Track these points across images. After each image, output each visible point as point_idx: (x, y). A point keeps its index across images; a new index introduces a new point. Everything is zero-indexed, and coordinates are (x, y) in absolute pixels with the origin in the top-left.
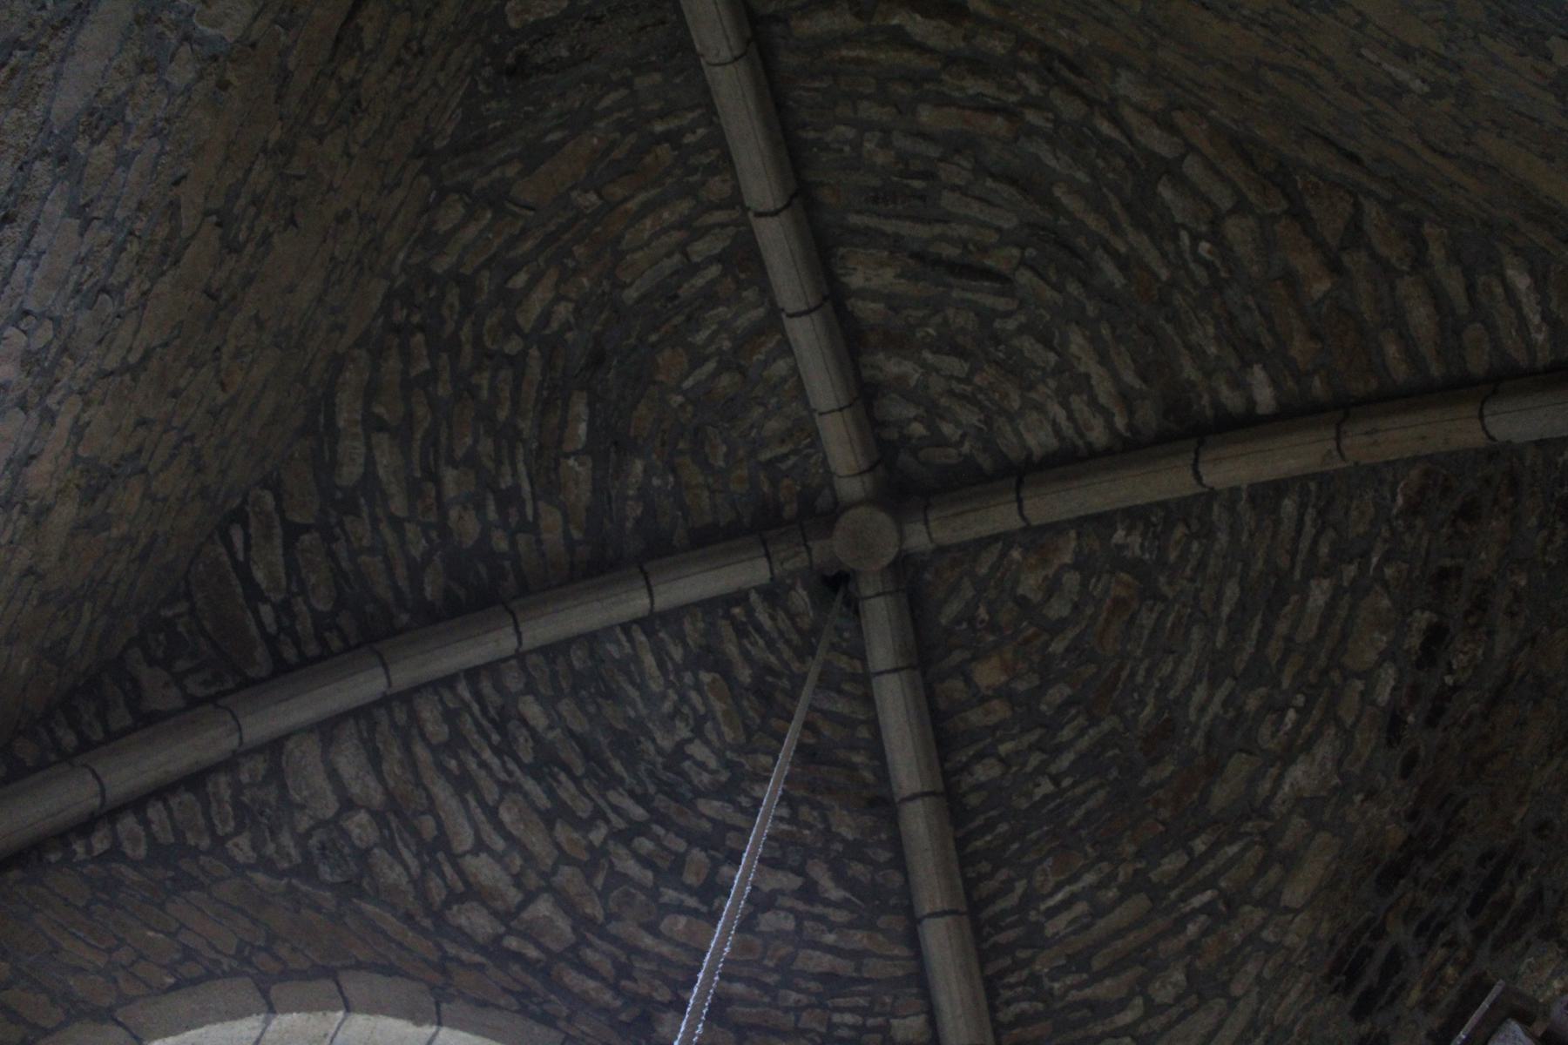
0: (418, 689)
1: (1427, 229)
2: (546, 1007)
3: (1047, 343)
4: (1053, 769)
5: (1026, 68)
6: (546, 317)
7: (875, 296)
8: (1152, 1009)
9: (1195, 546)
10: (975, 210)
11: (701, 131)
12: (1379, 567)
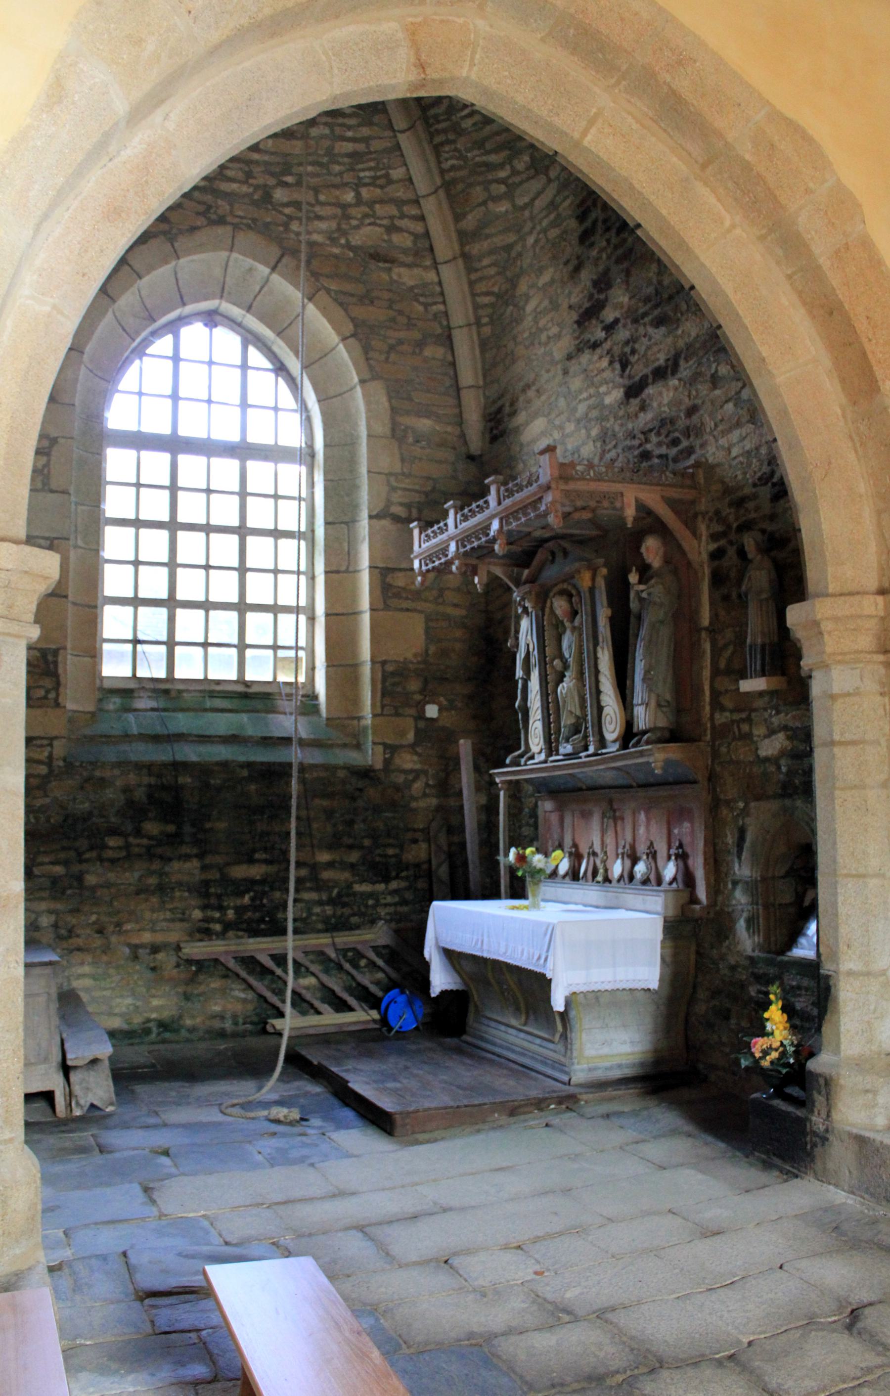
8: (515, 172)
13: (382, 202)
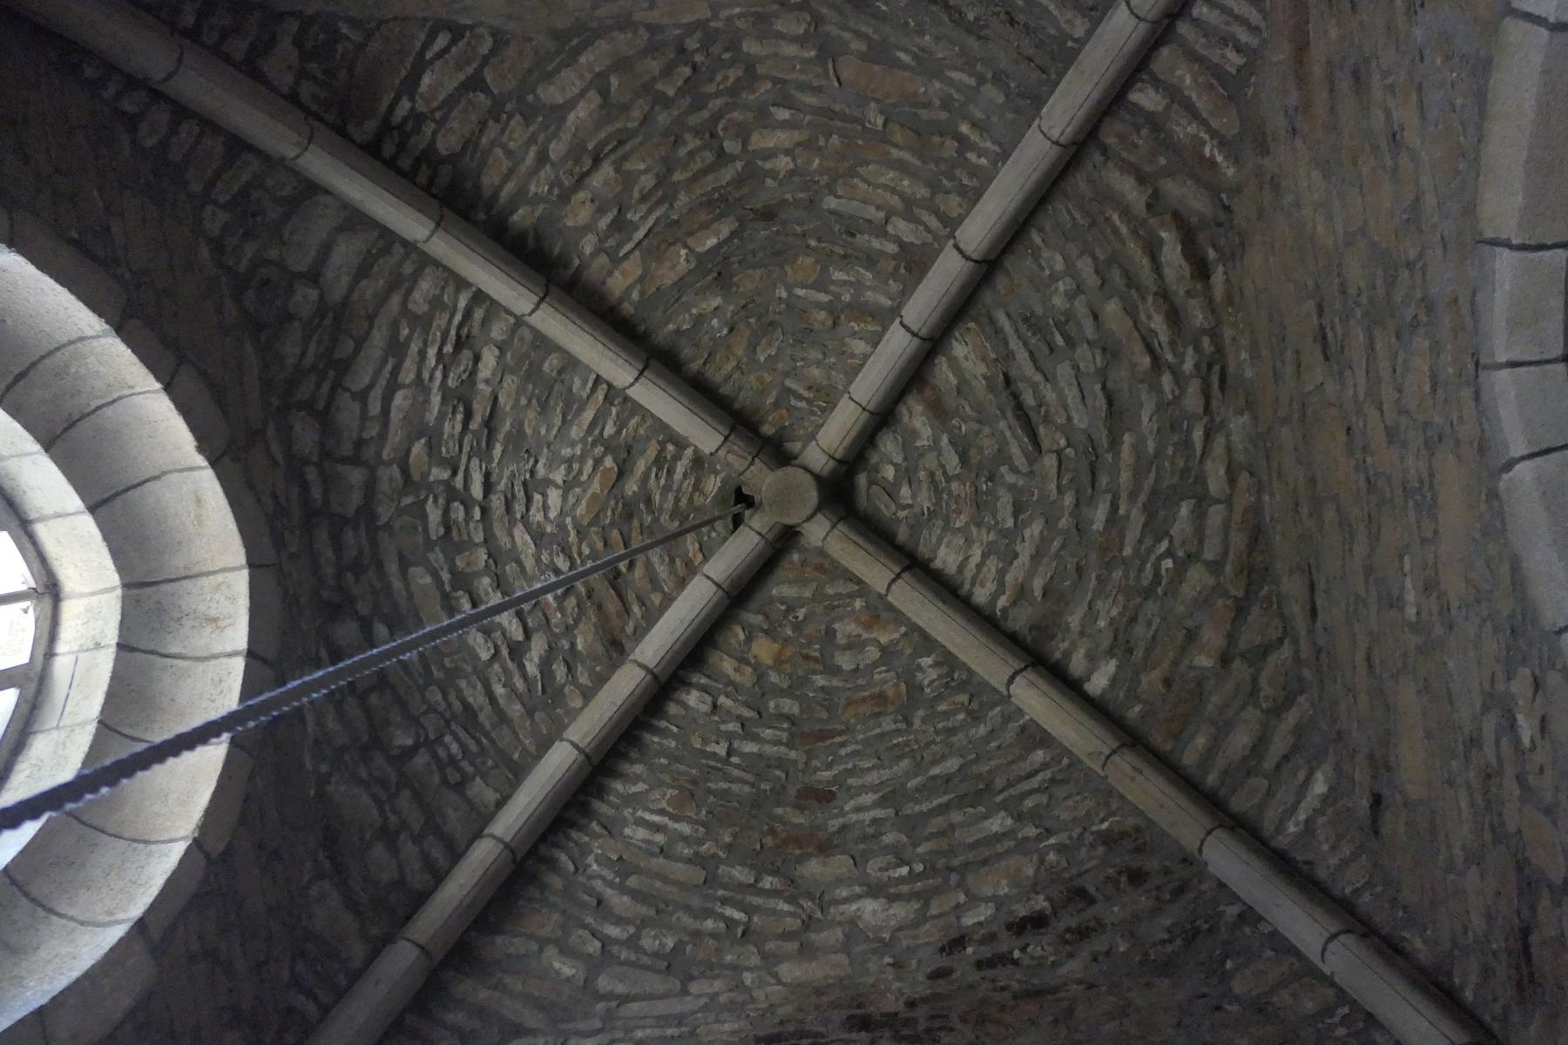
0: (437, 264)
2: (287, 534)
3: (1017, 510)
5: (1197, 349)
6: (770, 154)
8: (632, 942)
9: (961, 716)
10: (1072, 394)
11: (983, 161)
13: (418, 796)
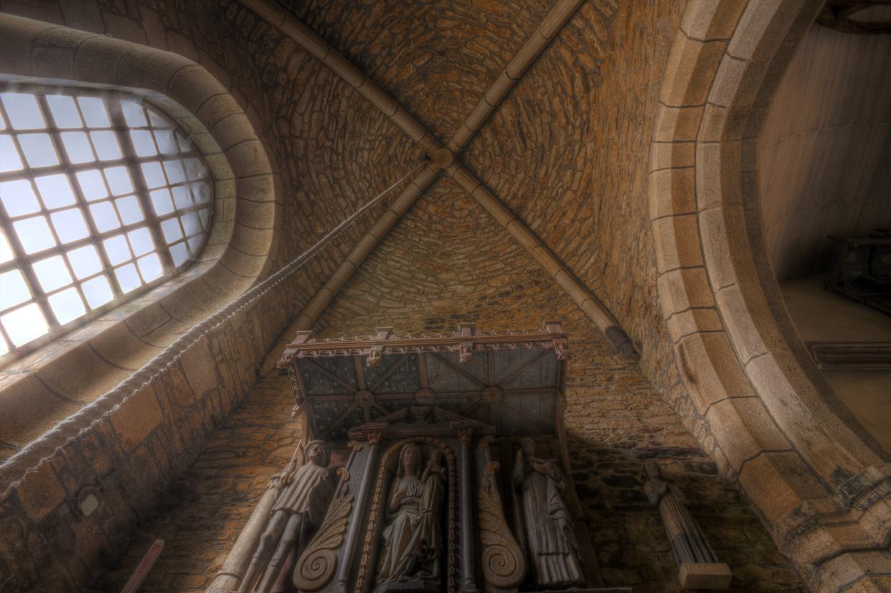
0: (327, 66)
1: (593, 235)
4: (422, 238)
5: (582, 118)
6: (444, 30)
7: (503, 119)
10: (539, 129)
11: (520, 40)
12: (513, 274)
